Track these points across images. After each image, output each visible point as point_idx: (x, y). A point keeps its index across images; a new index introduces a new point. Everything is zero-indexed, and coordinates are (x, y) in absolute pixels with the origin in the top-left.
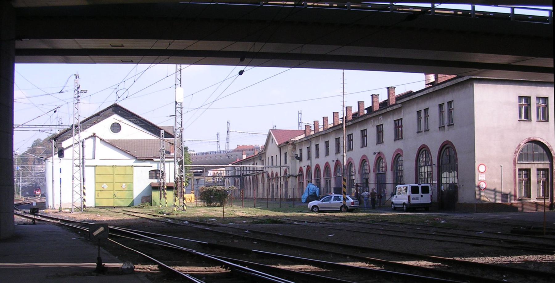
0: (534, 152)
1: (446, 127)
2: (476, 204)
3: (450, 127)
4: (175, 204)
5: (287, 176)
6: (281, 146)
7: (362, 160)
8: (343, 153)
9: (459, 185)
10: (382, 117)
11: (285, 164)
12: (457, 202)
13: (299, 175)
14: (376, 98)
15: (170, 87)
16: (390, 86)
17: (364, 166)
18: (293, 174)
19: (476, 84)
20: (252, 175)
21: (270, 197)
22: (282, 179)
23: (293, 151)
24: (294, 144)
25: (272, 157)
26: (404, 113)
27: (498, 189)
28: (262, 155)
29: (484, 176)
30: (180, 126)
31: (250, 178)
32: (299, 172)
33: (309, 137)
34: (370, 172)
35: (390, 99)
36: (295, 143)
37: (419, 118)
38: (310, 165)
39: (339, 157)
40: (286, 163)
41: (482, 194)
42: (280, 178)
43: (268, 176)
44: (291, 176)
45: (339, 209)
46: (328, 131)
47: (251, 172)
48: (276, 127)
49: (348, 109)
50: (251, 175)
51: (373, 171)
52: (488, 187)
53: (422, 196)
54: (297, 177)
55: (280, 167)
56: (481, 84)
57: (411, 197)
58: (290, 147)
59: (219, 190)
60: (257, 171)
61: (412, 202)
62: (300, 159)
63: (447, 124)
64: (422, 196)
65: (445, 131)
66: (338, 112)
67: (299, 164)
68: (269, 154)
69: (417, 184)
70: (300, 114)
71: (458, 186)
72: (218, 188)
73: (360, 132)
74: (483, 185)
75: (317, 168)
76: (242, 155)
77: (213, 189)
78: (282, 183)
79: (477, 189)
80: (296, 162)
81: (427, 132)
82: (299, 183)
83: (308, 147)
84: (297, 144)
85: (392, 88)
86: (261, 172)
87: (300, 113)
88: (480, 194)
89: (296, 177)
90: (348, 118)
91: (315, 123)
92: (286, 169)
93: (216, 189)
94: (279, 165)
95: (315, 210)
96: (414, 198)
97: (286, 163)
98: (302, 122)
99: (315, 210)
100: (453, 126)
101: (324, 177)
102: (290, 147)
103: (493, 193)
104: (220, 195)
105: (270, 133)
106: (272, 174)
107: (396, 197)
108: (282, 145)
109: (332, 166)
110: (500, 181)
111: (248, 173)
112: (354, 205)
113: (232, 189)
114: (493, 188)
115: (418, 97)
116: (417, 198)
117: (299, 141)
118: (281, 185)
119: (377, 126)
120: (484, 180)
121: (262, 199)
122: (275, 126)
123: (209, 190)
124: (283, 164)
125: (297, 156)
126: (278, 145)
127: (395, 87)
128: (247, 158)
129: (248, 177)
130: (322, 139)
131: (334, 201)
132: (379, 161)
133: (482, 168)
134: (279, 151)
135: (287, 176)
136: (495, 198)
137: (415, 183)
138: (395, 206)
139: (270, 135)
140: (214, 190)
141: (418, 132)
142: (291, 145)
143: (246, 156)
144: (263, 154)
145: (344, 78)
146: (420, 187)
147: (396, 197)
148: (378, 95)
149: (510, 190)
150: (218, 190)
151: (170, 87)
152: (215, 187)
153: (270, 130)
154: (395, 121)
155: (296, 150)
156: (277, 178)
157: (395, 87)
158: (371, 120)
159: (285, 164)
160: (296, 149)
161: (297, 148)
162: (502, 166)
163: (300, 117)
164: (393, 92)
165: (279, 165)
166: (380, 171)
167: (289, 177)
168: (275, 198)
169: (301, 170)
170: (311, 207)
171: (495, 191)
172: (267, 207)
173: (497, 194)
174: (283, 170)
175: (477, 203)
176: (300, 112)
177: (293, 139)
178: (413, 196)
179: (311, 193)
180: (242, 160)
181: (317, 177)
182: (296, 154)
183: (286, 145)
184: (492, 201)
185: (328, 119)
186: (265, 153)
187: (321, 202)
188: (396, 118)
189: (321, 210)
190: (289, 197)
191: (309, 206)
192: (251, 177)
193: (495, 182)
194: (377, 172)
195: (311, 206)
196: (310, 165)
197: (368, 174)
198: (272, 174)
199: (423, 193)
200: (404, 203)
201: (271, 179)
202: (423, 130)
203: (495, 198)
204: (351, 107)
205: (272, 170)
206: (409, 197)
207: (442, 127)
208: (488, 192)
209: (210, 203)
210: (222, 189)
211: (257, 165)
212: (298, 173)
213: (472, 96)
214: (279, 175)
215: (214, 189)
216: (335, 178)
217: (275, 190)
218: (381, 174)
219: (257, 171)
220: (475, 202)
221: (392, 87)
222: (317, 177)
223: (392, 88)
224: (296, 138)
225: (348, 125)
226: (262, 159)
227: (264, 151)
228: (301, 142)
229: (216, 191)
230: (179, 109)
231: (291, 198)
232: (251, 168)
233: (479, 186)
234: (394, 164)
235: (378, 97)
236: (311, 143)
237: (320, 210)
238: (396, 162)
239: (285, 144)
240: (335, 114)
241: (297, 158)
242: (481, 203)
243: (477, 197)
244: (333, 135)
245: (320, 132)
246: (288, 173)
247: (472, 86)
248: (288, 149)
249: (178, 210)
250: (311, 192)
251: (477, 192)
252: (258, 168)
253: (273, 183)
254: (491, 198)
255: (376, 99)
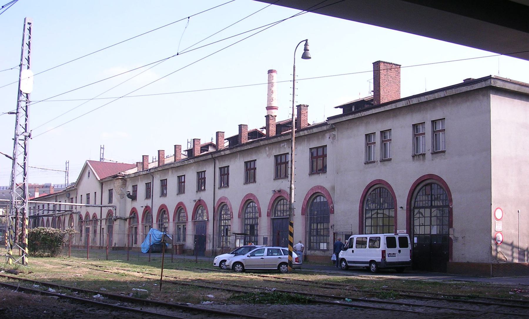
0: (91, 219)
1: (429, 155)
2: (493, 265)
3: (434, 155)
4: (11, 253)
5: (111, 219)
6: (104, 181)
7: (246, 200)
8: (291, 184)
9: (454, 237)
10: (287, 144)
11: (108, 203)
12: (450, 261)
13: (130, 218)
14: (272, 120)
15: (12, 69)
16: (302, 104)
17: (247, 207)
18: (121, 216)
19: (493, 95)
20: (52, 216)
21: (82, 243)
22: (104, 222)
23: (122, 187)
24: (124, 179)
25: (88, 195)
26: (337, 138)
27: (516, 243)
28: (71, 193)
29: (501, 224)
30: (24, 131)
31: (48, 220)
32: (131, 214)
33: (151, 170)
34: (260, 216)
35: (302, 120)
36: (126, 177)
37: (367, 144)
38: (151, 207)
39: (182, 198)
40: (110, 201)
41: (499, 249)
42: (100, 221)
43: (81, 218)
44: (119, 218)
45: (277, 268)
46: (186, 162)
47: (51, 213)
48: (68, 163)
49: (219, 135)
50: (49, 216)
51: (300, 211)
52: (505, 240)
53: (400, 251)
54: (126, 221)
55: (101, 207)
56: (498, 96)
57: (386, 253)
58: (118, 183)
59: (50, 234)
60: (60, 211)
61: (388, 259)
62: (133, 197)
63: (431, 151)
64: (400, 251)
65: (426, 161)
66: (200, 140)
67: (130, 205)
68: (82, 190)
69: (393, 234)
70: (102, 149)
71: (452, 238)
72: (48, 230)
73: (243, 164)
74: (500, 237)
75: (163, 210)
76: (35, 192)
77: (40, 232)
78: (102, 227)
79: (493, 242)
80: (125, 200)
81: (386, 163)
82: (129, 228)
83: (133, 185)
84: (128, 179)
85: (305, 106)
86: (70, 213)
87: (102, 148)
88: (496, 250)
89: (126, 220)
90: (219, 147)
91: (160, 152)
92: (110, 211)
93: (45, 232)
94: (98, 203)
95: (284, 270)
96: (390, 254)
97: (110, 201)
98: (104, 158)
99: (239, 268)
100: (443, 154)
101: (174, 220)
102: (118, 183)
103: (510, 248)
104: (52, 241)
105: (87, 163)
106: (87, 214)
107: (353, 251)
108: (106, 180)
109: (235, 206)
110: (518, 233)
111: (46, 213)
112: (298, 262)
113: (71, 233)
114: (510, 241)
115: (338, 122)
116: (394, 254)
117: (133, 176)
118: (102, 229)
119: (276, 156)
120: (501, 231)
121: (101, 248)
122: (67, 162)
123: (34, 233)
124: (106, 202)
125: (130, 193)
126: (99, 179)
127: (308, 106)
128: (40, 196)
129: (45, 219)
130: (172, 173)
131: (267, 255)
132: (277, 202)
133: (499, 214)
134: (101, 186)
135: (111, 219)
136: (512, 255)
137: (359, 234)
138: (349, 264)
139: (86, 166)
140: (42, 233)
141: (367, 163)
142: (120, 181)
143: (39, 195)
144: (73, 191)
145: (296, 74)
146: (397, 237)
147: (353, 251)
148: (276, 116)
149: (527, 244)
150: (47, 234)
151: (12, 69)
152: (44, 230)
153: (88, 162)
154: (311, 149)
155: (126, 186)
156: (95, 219)
157: (308, 106)
158: (265, 148)
159: (108, 203)
160: (127, 185)
161: (127, 183)
162: (519, 211)
163: (102, 152)
164: (305, 112)
165: (100, 204)
166: (180, 220)
167: (115, 220)
168: (90, 245)
169: (134, 211)
170: (232, 263)
171: (511, 245)
172: (128, 260)
173: (515, 250)
174: (105, 211)
175: (493, 262)
176: (102, 147)
177: (123, 173)
178: (389, 251)
179: (155, 240)
180: (34, 198)
181: (160, 221)
182: (128, 192)
183: (112, 180)
184: (509, 259)
185: (181, 148)
186: (76, 189)
187: (248, 256)
188: (315, 144)
189: (246, 268)
190: (115, 245)
191: (215, 261)
192: (51, 218)
193: (512, 233)
194: (274, 216)
195: (231, 262)
196: (151, 207)
197: (258, 218)
198: (87, 214)
199: (400, 247)
200: (372, 262)
201: (84, 221)
202: (379, 160)
203: (512, 255)
204: (224, 132)
205: (86, 210)
206: (384, 252)
207: (418, 155)
208: (505, 246)
209: (35, 252)
210: (55, 232)
211: (76, 203)
212: (128, 215)
213: (488, 111)
214: (99, 217)
215: (42, 231)
216: (195, 222)
217: (90, 235)
218: (281, 220)
219: (60, 211)
220: (490, 262)
221: (304, 106)
222: (160, 221)
223: (305, 106)
224: (127, 171)
225: (224, 154)
226: (71, 197)
227: (75, 187)
228: (136, 176)
229: (46, 234)
230: (23, 104)
231: (117, 246)
232: (62, 206)
233: (495, 239)
234: (308, 206)
235: (275, 119)
236: (153, 178)
237: (245, 268)
238: (310, 203)
239: (111, 179)
240: (197, 141)
241: (129, 196)
242: (497, 263)
243: (494, 253)
244: (193, 168)
245: (166, 165)
246: (114, 215)
247: (485, 98)
248: (115, 185)
249: (15, 263)
250: (156, 239)
251: (494, 247)
252: (66, 206)
253: (89, 227)
254: (507, 255)
255: (273, 122)
